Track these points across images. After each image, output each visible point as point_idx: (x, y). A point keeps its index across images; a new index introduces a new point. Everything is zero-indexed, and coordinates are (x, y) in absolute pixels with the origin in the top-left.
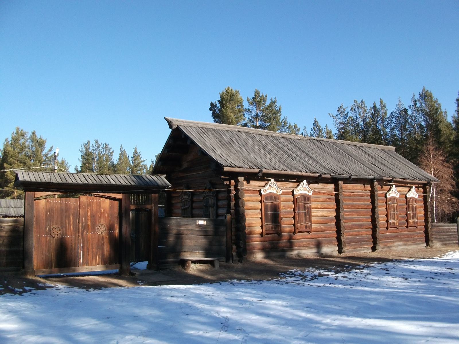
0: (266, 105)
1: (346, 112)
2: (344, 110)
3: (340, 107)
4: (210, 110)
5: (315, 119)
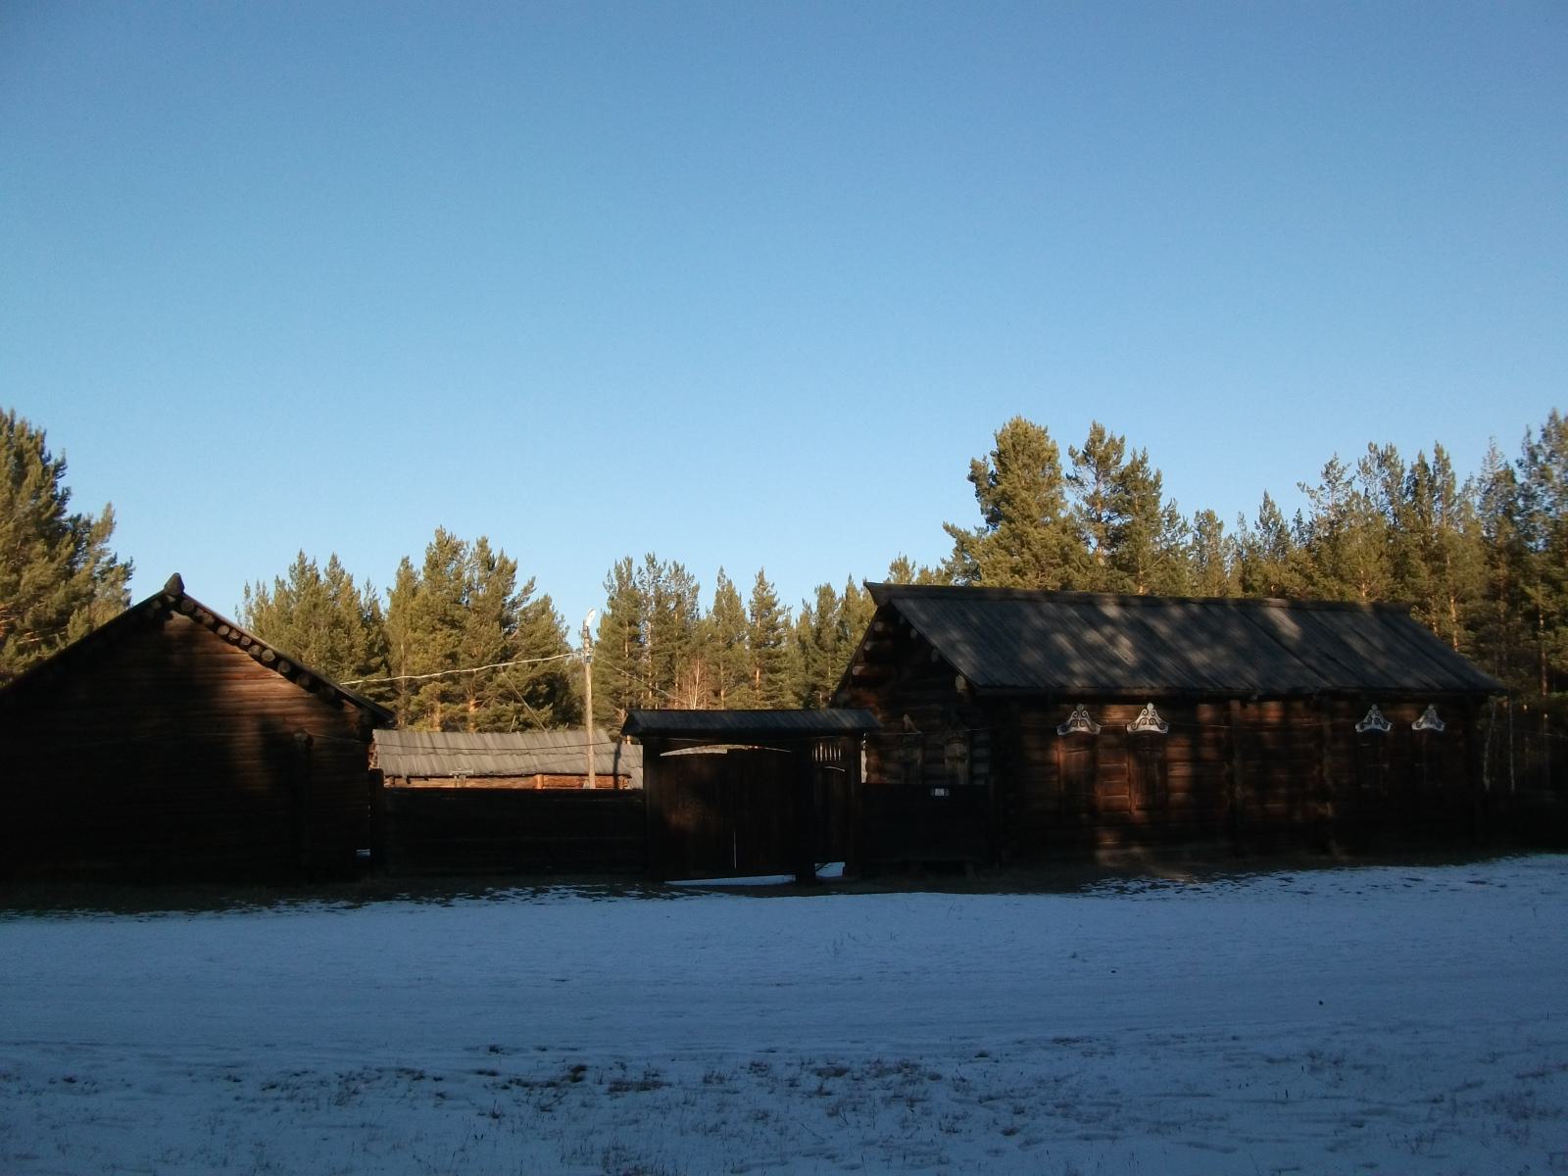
0: (1121, 464)
1: (1346, 478)
2: (1342, 472)
3: (1331, 463)
4: (972, 478)
5: (1266, 496)
